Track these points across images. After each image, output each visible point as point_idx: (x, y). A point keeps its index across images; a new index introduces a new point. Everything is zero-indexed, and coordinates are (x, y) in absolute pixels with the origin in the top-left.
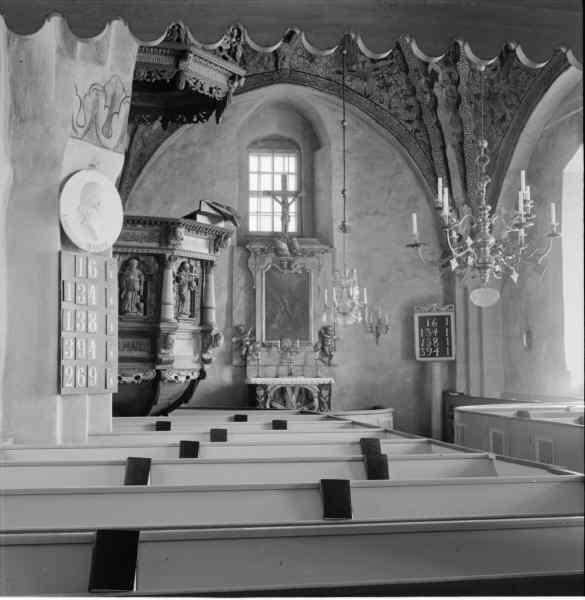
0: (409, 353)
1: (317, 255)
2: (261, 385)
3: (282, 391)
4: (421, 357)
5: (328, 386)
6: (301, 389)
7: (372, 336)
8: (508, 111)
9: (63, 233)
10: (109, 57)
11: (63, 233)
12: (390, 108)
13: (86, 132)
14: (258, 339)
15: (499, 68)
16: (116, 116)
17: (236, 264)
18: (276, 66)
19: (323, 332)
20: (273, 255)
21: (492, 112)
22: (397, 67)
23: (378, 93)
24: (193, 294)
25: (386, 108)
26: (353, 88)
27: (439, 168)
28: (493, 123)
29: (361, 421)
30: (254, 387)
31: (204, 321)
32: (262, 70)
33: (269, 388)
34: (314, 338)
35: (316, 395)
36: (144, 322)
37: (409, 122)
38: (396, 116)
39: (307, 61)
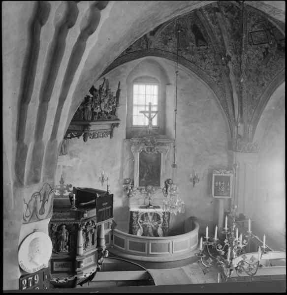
0: (209, 192)
2: (135, 212)
5: (169, 214)
7: (192, 183)
8: (266, 82)
9: (21, 269)
10: (42, 172)
11: (21, 269)
12: (205, 68)
13: (30, 219)
15: (263, 59)
16: (46, 202)
17: (125, 149)
18: (147, 47)
19: (167, 182)
21: (258, 81)
22: (210, 50)
23: (199, 62)
24: (93, 235)
25: (204, 69)
26: (186, 58)
27: (230, 104)
28: (258, 85)
30: (132, 213)
31: (99, 246)
32: (140, 49)
33: (139, 214)
34: (163, 185)
36: (69, 254)
37: (215, 77)
38: (209, 73)
39: (163, 44)
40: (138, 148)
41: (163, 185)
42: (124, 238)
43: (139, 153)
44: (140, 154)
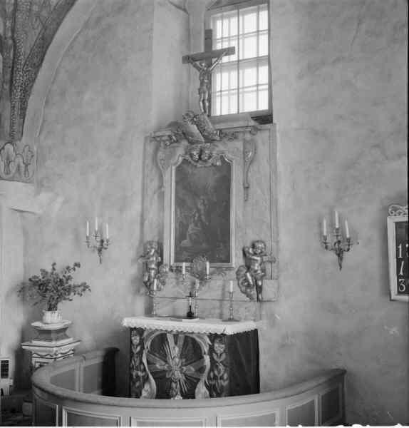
1: (240, 136)
3: (161, 338)
4: (399, 293)
6: (186, 337)
7: (332, 256)
14: (166, 261)
20: (185, 143)
29: (90, 399)
33: (145, 334)
34: (237, 260)
35: (206, 349)
40: (172, 155)
41: (237, 260)
42: (82, 369)
43: (174, 168)
44: (179, 170)
